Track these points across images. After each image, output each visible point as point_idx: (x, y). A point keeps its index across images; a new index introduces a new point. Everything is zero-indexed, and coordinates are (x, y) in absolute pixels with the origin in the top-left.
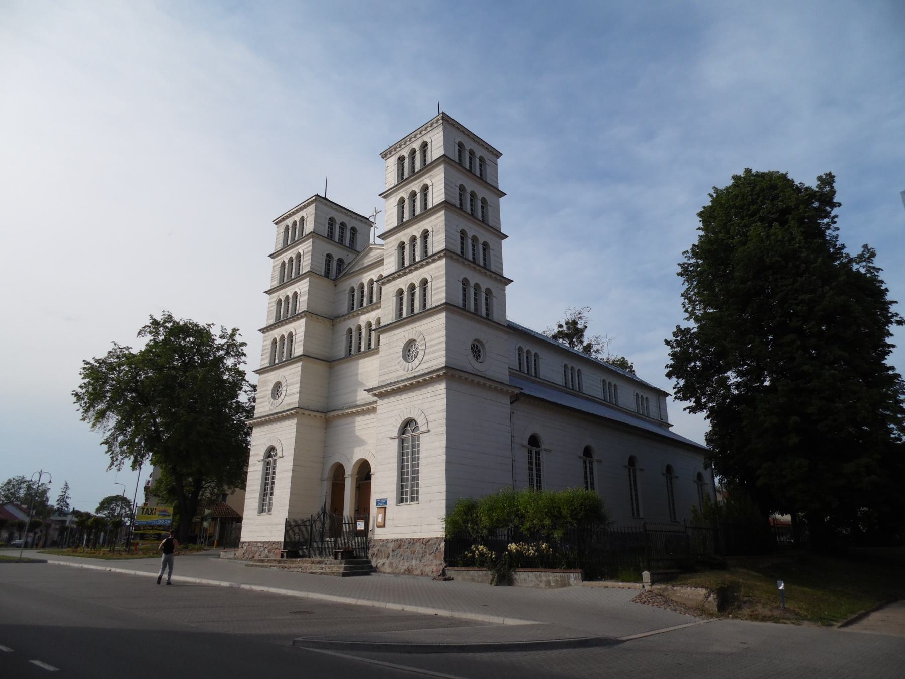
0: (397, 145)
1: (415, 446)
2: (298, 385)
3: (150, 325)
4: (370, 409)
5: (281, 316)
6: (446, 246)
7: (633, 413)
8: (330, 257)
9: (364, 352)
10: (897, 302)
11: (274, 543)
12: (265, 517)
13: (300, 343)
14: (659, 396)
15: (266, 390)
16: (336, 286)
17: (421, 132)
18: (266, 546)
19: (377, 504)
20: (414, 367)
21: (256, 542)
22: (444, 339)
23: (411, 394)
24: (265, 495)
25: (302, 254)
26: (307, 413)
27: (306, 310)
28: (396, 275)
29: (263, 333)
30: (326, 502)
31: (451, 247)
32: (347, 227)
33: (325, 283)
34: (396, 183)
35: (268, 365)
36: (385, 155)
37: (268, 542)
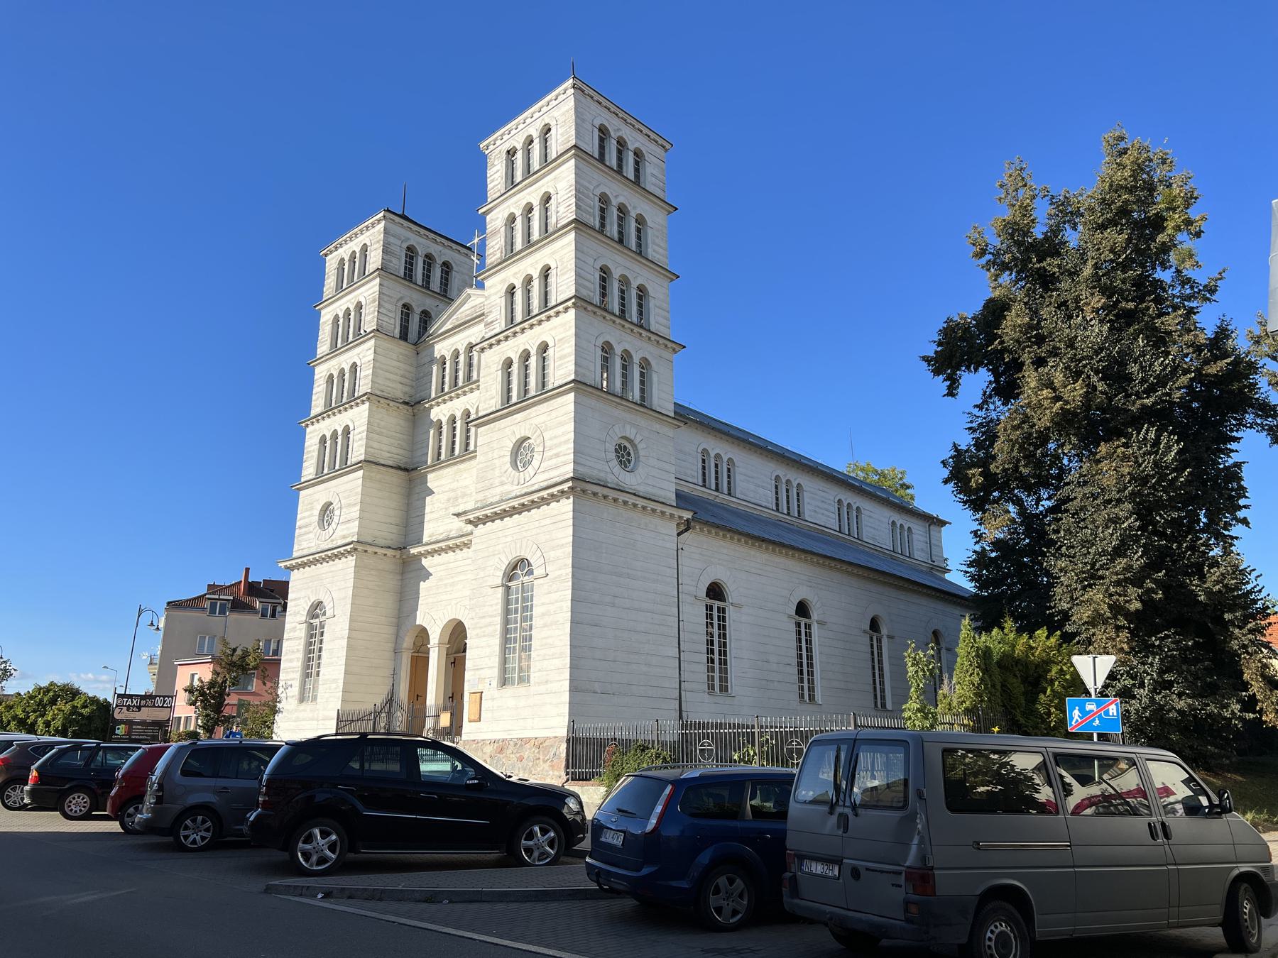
1: (527, 600)
4: (461, 544)
5: (333, 401)
7: (886, 551)
8: (408, 309)
9: (459, 456)
10: (950, 524)
12: (307, 706)
13: (360, 442)
15: (311, 515)
20: (527, 479)
22: (572, 435)
25: (364, 304)
26: (370, 549)
27: (369, 391)
28: (501, 337)
31: (584, 293)
33: (403, 348)
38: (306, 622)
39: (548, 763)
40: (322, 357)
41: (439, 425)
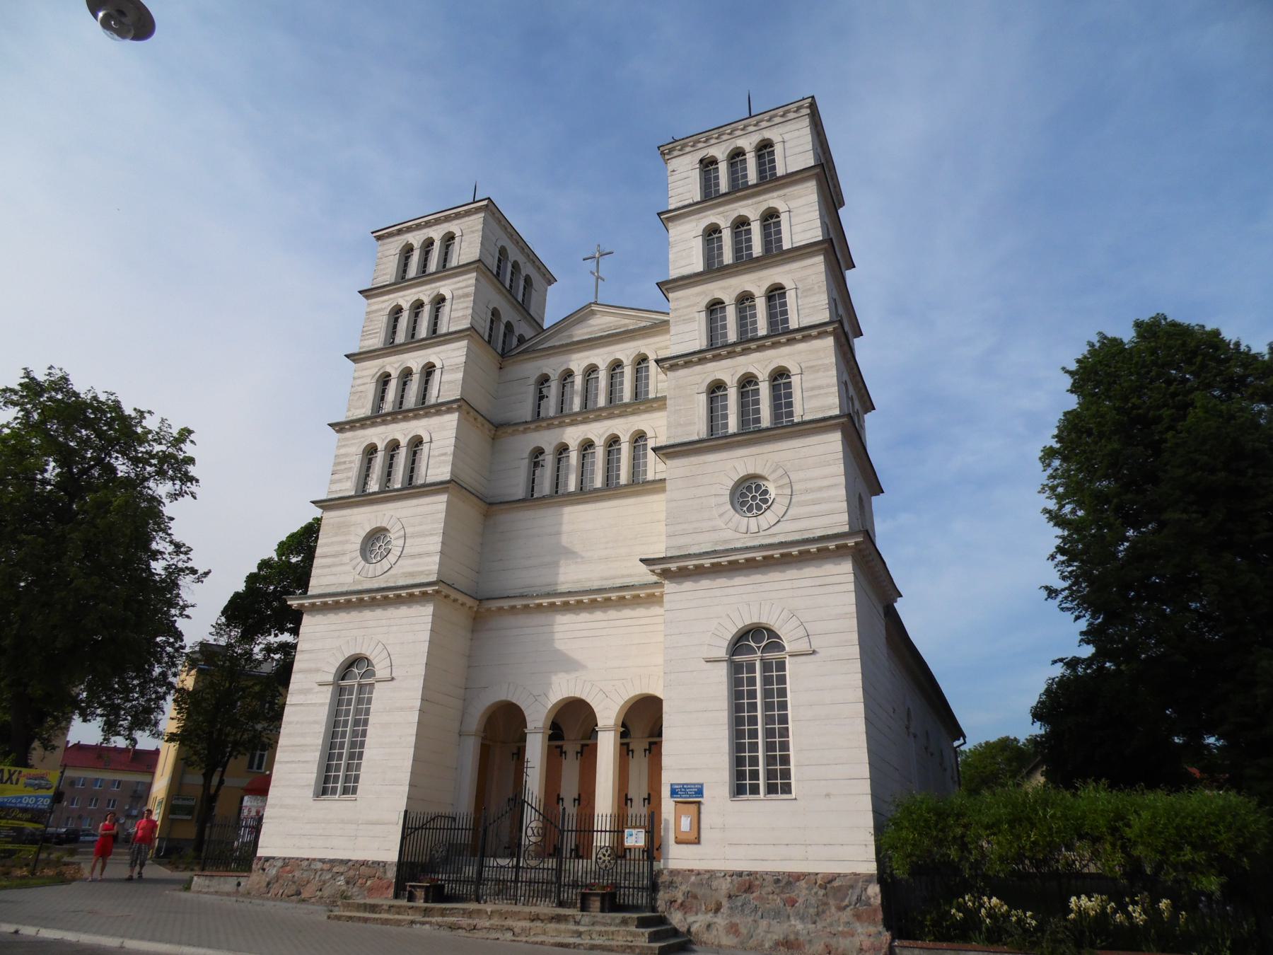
0: (713, 132)
1: (364, 702)
2: (439, 539)
3: (18, 388)
11: (364, 863)
12: (336, 806)
16: (501, 368)
17: (758, 123)
18: (341, 869)
19: (674, 792)
23: (757, 578)
29: (337, 432)
32: (520, 273)
34: (393, 281)
35: (353, 493)
36: (381, 236)
39: (849, 912)
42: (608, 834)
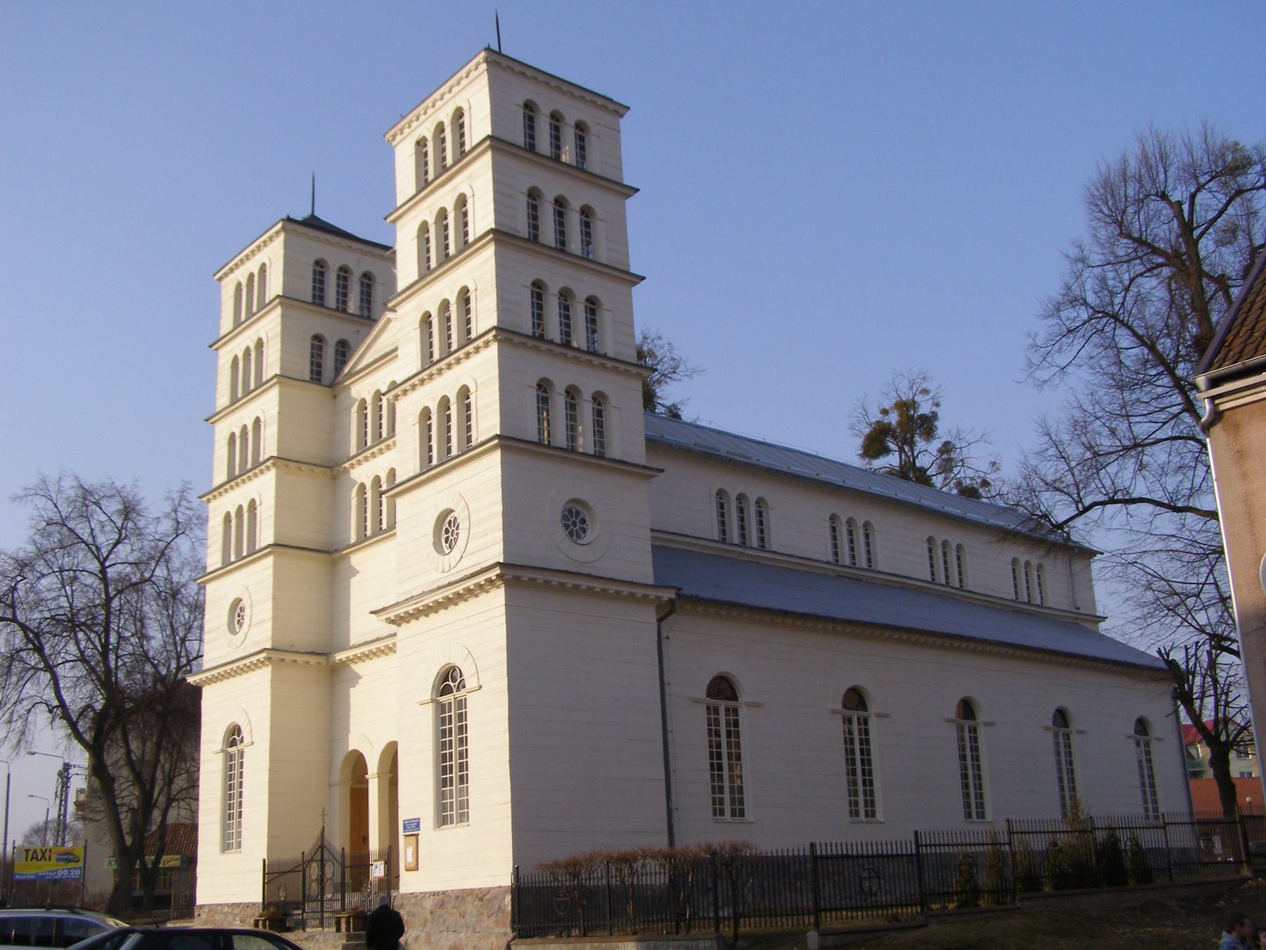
6: (499, 320)
12: (231, 857)
14: (1070, 560)
18: (236, 911)
20: (453, 565)
21: (221, 904)
24: (230, 817)
28: (415, 381)
30: (323, 827)
37: (238, 905)
38: (222, 751)
40: (221, 412)
41: (362, 487)
42: (924, 843)
